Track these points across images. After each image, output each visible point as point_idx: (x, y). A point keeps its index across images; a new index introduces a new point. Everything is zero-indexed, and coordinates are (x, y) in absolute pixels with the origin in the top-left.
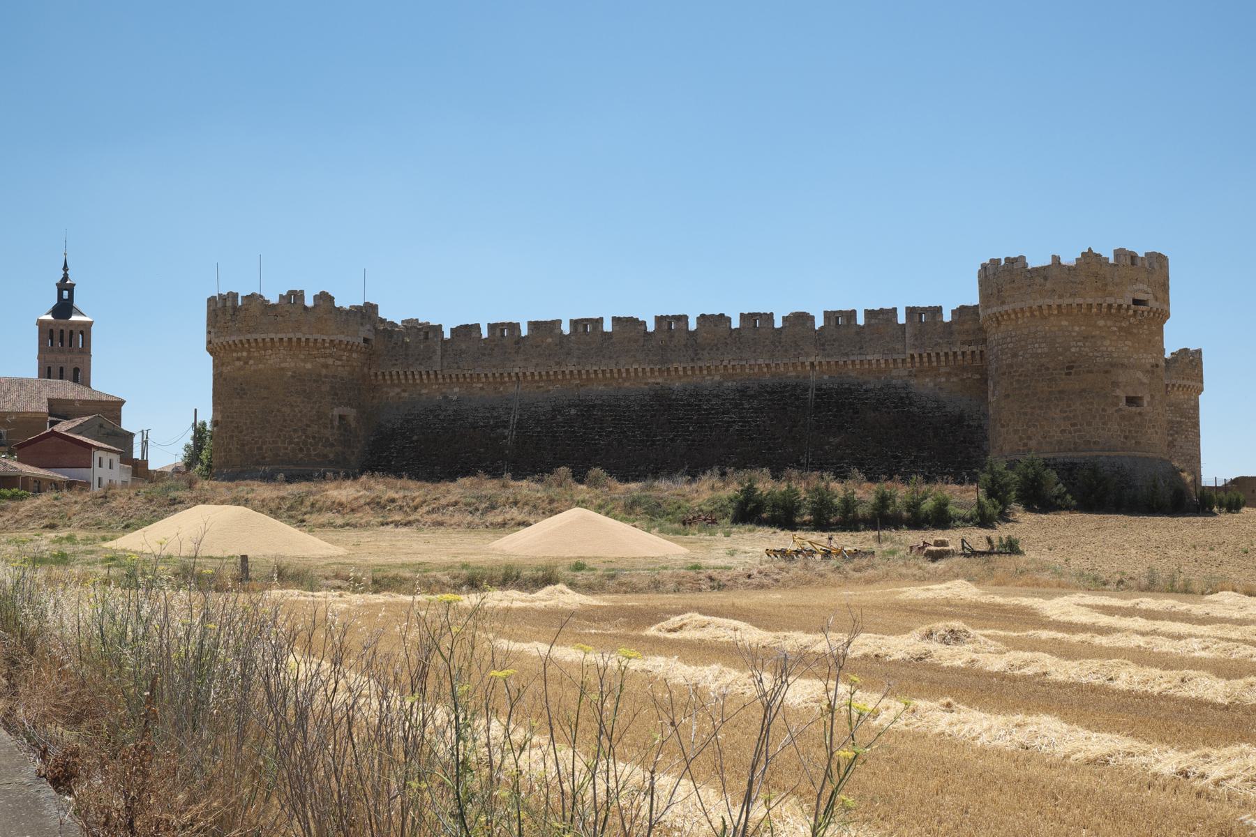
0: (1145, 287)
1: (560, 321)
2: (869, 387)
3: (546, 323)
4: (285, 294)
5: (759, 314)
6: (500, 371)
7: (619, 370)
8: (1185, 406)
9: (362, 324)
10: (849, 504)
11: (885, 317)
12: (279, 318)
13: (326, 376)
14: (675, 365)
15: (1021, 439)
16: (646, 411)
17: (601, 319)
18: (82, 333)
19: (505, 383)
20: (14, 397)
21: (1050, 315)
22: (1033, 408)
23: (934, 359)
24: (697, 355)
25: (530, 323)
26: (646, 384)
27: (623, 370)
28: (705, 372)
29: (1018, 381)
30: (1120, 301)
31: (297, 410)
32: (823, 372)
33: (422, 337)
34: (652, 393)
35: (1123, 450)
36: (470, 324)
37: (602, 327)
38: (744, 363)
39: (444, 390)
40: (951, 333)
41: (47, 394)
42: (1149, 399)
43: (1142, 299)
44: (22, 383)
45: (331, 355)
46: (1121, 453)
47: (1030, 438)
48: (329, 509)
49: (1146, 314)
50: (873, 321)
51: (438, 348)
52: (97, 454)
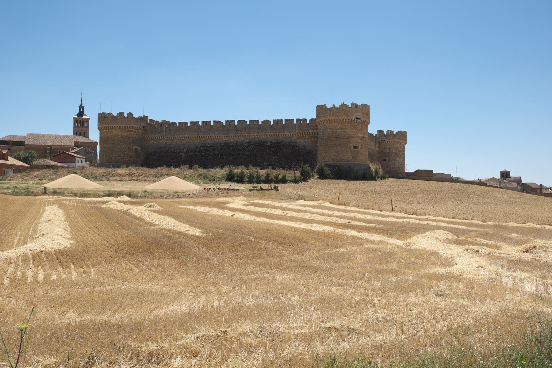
0: (360, 114)
1: (199, 122)
2: (286, 142)
3: (195, 122)
4: (118, 113)
5: (255, 120)
6: (182, 136)
7: (215, 136)
8: (400, 148)
9: (142, 122)
10: (258, 177)
11: (290, 121)
12: (117, 120)
13: (131, 137)
14: (231, 135)
15: (324, 158)
16: (222, 148)
17: (211, 121)
18: (86, 121)
19: (183, 139)
20: (64, 141)
21: (332, 122)
22: (327, 149)
23: (304, 134)
24: (237, 132)
25: (214, 121)
26: (223, 140)
27: (216, 136)
28: (239, 137)
29: (323, 141)
30: (352, 118)
31: (122, 147)
32: (273, 138)
33: (160, 126)
34: (224, 143)
35: (352, 161)
36: (240, 120)
37: (211, 123)
38: (250, 134)
39: (166, 142)
40: (309, 127)
41: (75, 140)
42: (361, 147)
43: (359, 117)
44: (67, 137)
45: (132, 131)
46: (351, 162)
47: (326, 158)
48: (117, 176)
49: (360, 122)
50: (287, 123)
51: (164, 129)
52: (77, 159)
